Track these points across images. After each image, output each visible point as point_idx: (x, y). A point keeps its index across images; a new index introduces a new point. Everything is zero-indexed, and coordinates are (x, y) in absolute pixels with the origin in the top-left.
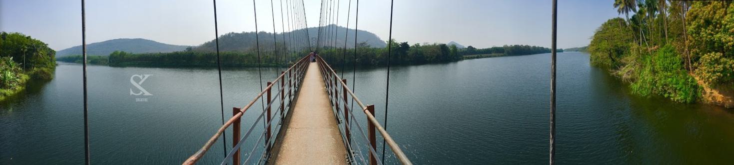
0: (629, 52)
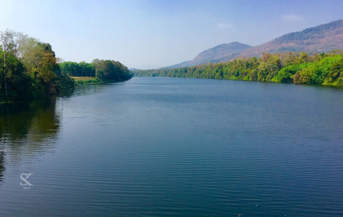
0: (254, 78)
